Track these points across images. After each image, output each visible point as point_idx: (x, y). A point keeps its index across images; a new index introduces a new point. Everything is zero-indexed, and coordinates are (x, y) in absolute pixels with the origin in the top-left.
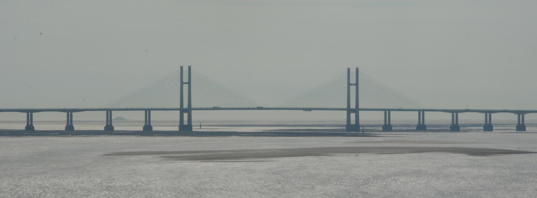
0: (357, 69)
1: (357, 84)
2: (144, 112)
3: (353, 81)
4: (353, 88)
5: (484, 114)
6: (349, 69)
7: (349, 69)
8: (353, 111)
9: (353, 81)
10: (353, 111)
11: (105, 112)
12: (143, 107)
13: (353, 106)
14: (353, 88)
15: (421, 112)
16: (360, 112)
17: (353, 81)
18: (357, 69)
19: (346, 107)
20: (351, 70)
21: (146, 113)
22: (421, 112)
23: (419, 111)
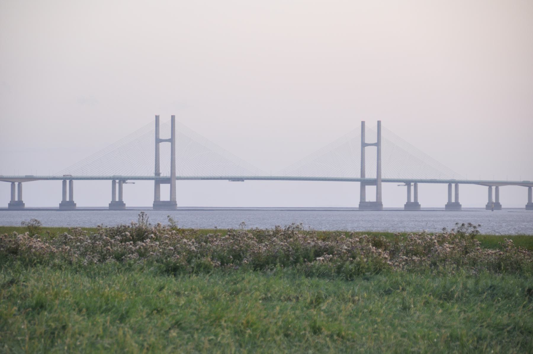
8: (166, 180)
10: (166, 180)
11: (447, 185)
13: (165, 172)
17: (371, 138)
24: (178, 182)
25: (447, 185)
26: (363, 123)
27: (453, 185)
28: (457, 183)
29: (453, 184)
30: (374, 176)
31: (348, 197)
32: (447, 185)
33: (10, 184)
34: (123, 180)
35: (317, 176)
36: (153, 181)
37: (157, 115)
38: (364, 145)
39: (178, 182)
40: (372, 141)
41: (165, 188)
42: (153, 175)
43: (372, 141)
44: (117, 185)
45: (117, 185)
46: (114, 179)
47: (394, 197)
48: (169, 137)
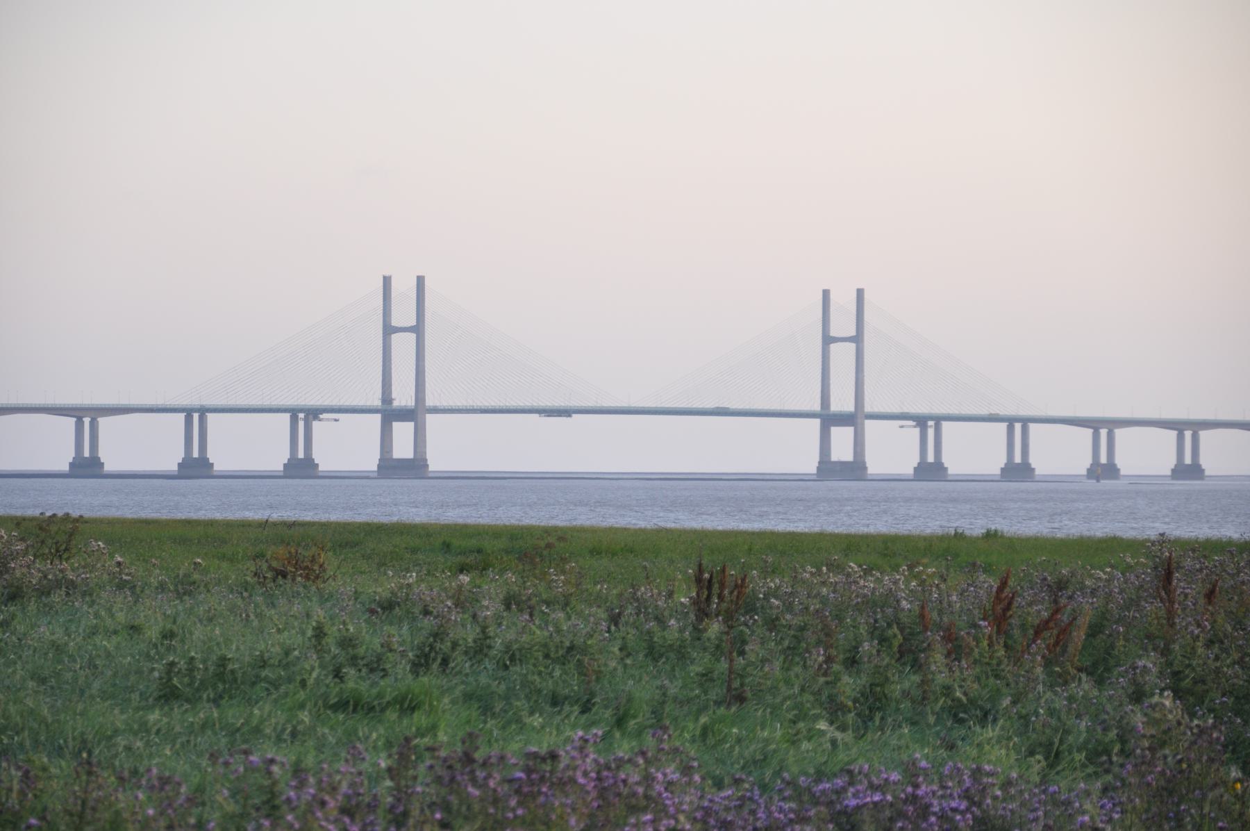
0: (420, 281)
1: (418, 329)
2: (287, 416)
3: (404, 315)
4: (403, 345)
5: (1174, 433)
6: (387, 281)
7: (387, 281)
8: (406, 415)
9: (404, 321)
10: (406, 415)
11: (182, 416)
12: (1003, 412)
13: (403, 397)
14: (403, 345)
15: (196, 416)
16: (428, 416)
17: (404, 315)
18: (420, 281)
19: (377, 402)
20: (428, 283)
21: (1011, 431)
22: (196, 416)
23: (188, 412)
24: (430, 418)
25: (1004, 426)
26: (826, 294)
27: (1018, 426)
28: (1026, 421)
29: (1019, 424)
30: (849, 407)
31: (793, 451)
32: (1004, 426)
33: (1174, 433)
34: (314, 413)
35: (124, 401)
36: (378, 417)
37: (387, 274)
38: (828, 340)
39: (430, 418)
40: (843, 331)
41: (403, 432)
42: (817, 407)
43: (843, 331)
44: (301, 424)
45: (301, 424)
46: (294, 412)
47: (891, 452)
48: (853, 333)
